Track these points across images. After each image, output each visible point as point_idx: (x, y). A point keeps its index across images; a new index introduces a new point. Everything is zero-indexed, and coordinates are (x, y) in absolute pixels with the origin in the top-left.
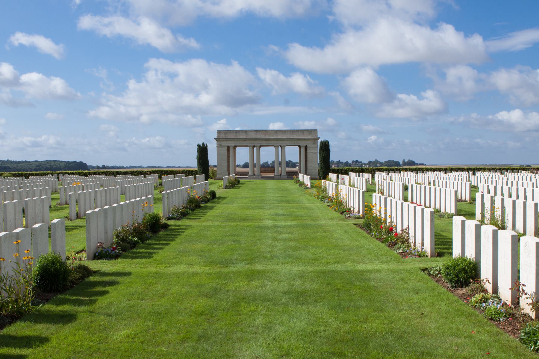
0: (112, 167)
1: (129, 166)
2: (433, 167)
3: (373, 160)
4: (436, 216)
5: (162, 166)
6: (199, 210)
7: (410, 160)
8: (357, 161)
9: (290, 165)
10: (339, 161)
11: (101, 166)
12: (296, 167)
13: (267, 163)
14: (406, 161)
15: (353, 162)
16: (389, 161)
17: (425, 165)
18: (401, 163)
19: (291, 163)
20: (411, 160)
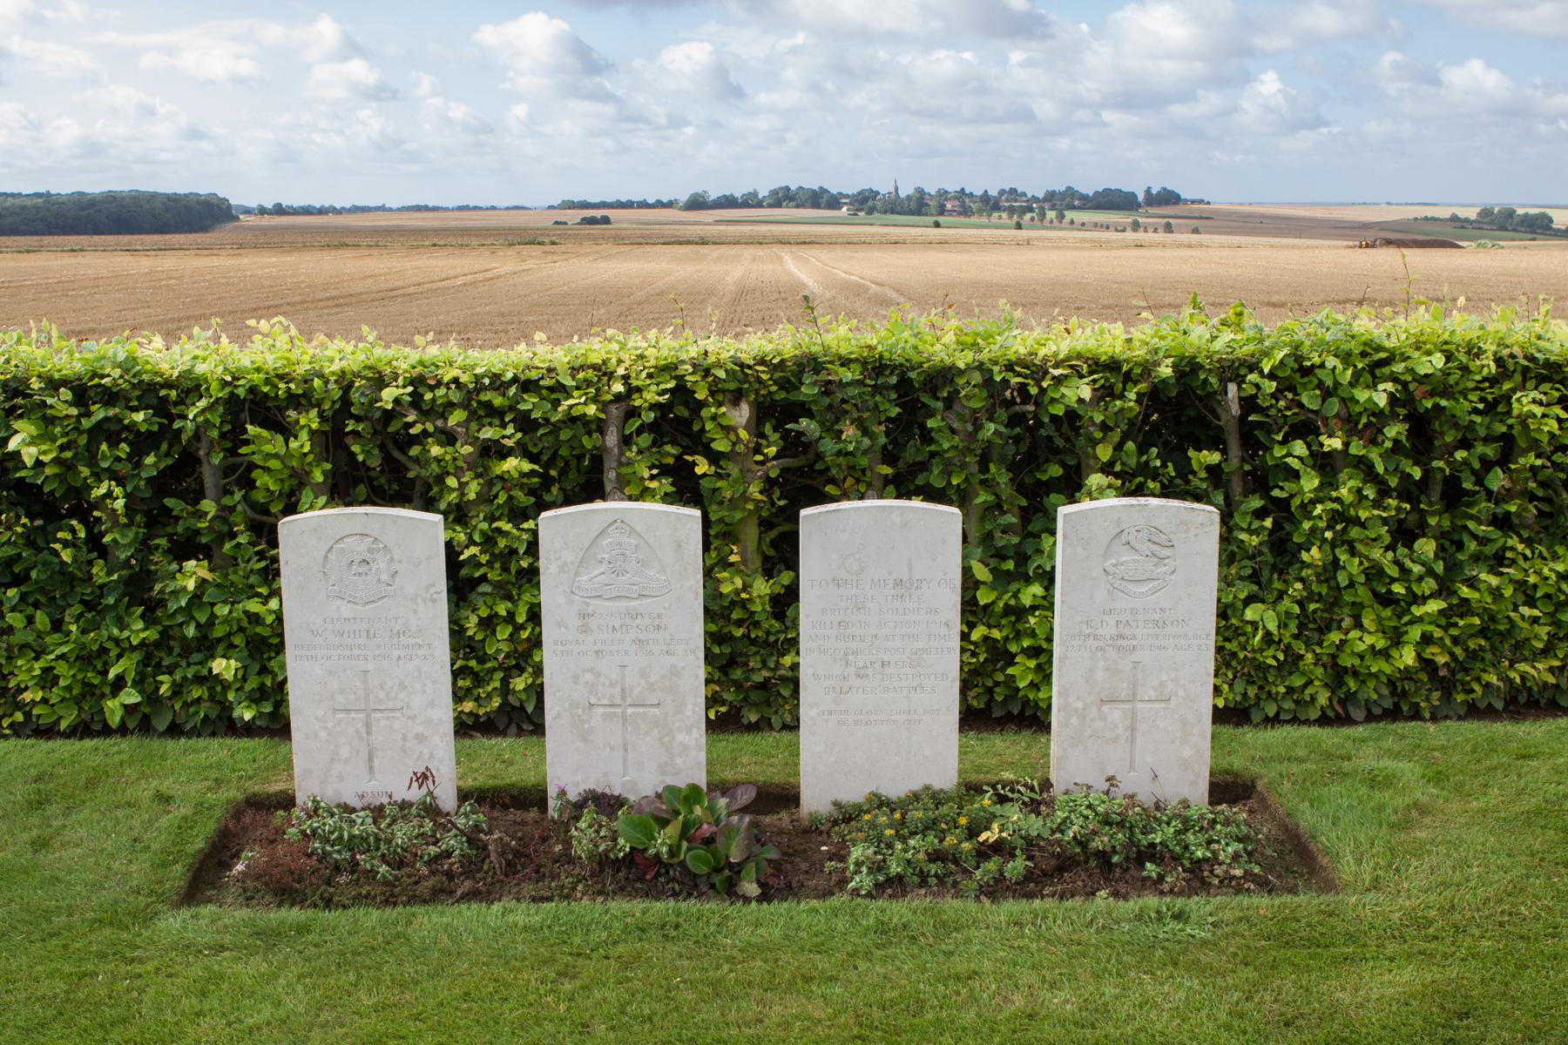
0: (302, 208)
1: (348, 206)
2: (1420, 238)
3: (1060, 187)
4: (196, 601)
5: (444, 205)
6: (1200, 272)
7: (1164, 189)
8: (1013, 191)
9: (823, 201)
10: (963, 189)
11: (270, 207)
12: (840, 208)
13: (755, 194)
14: (1154, 191)
15: (1002, 192)
16: (1105, 190)
17: (1209, 203)
18: (1141, 198)
19: (826, 196)
20: (1170, 188)
